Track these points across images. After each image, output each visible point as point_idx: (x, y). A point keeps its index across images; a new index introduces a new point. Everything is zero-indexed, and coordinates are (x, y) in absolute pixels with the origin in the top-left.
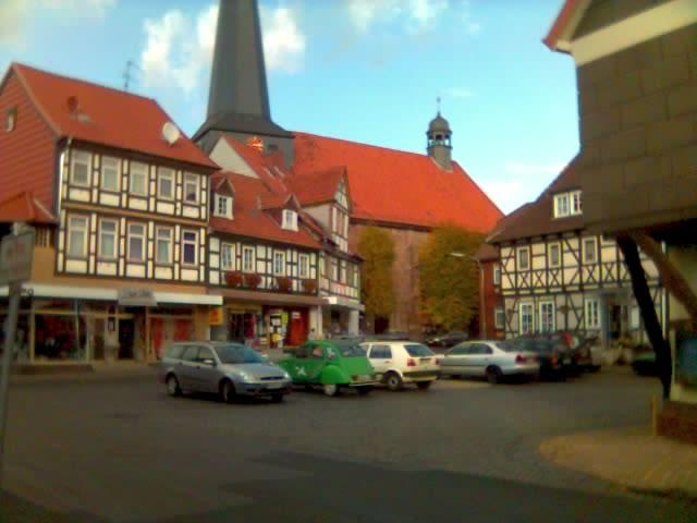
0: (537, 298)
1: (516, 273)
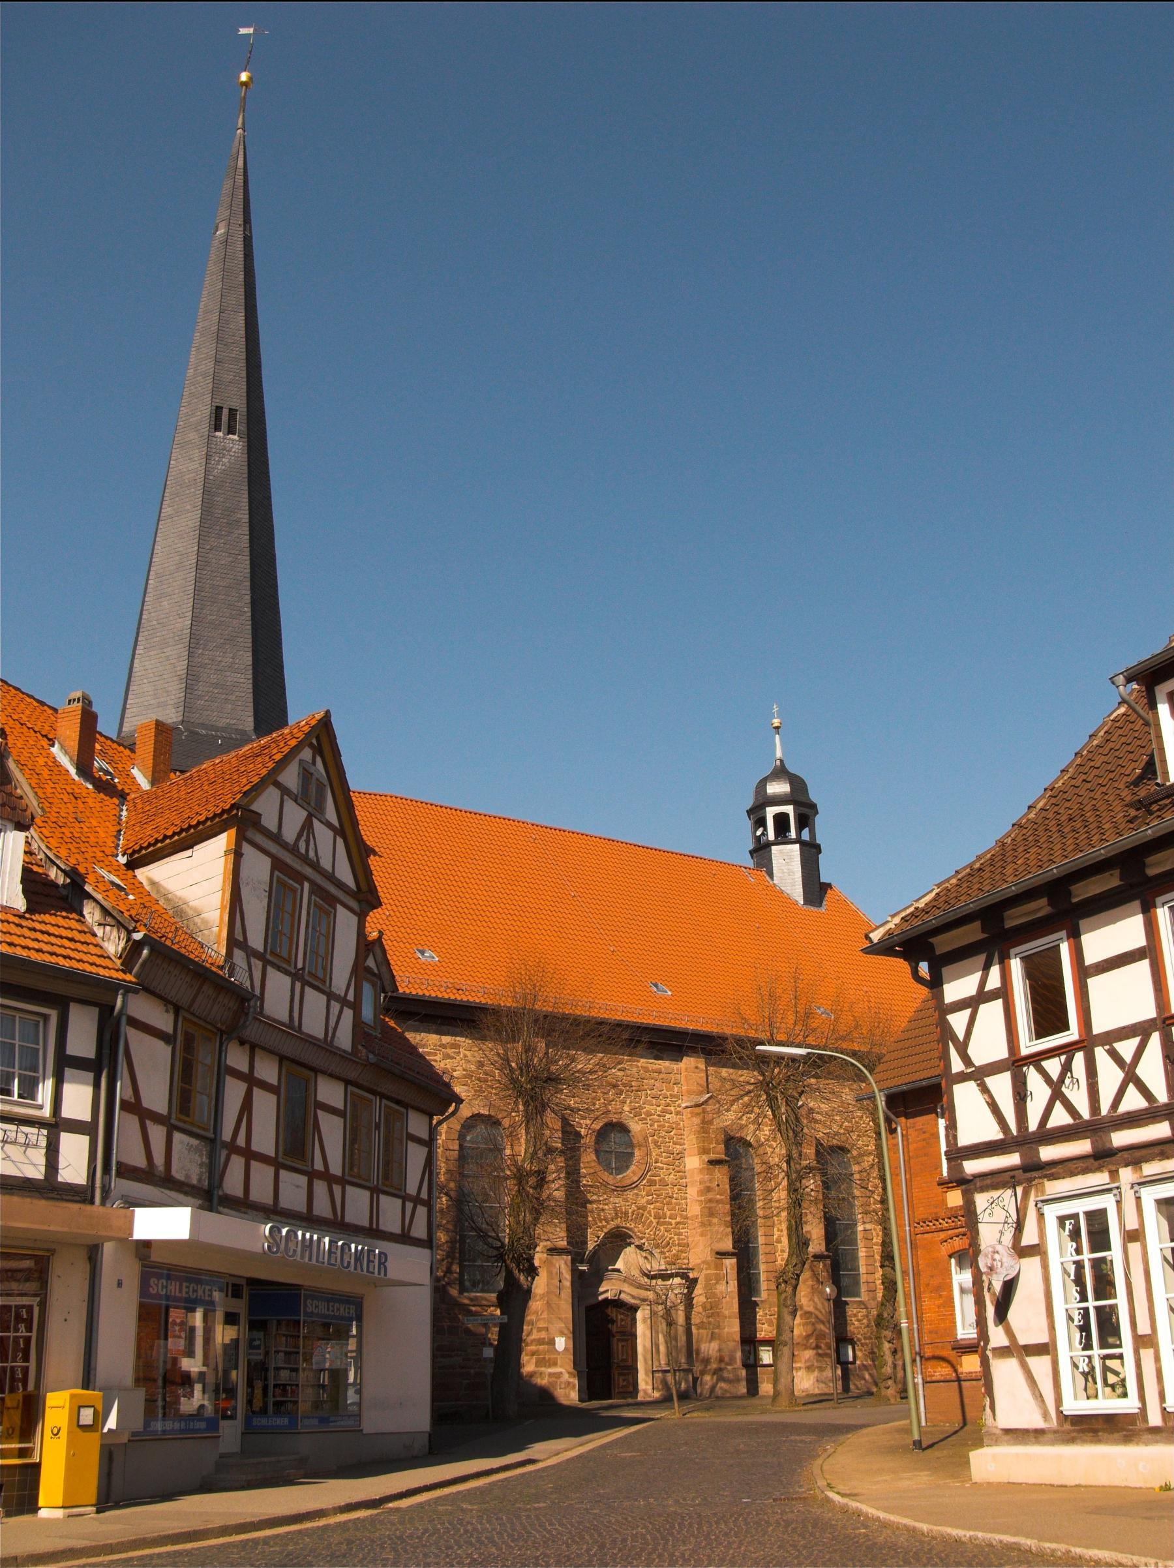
0: (1127, 1175)
1: (1016, 1064)
